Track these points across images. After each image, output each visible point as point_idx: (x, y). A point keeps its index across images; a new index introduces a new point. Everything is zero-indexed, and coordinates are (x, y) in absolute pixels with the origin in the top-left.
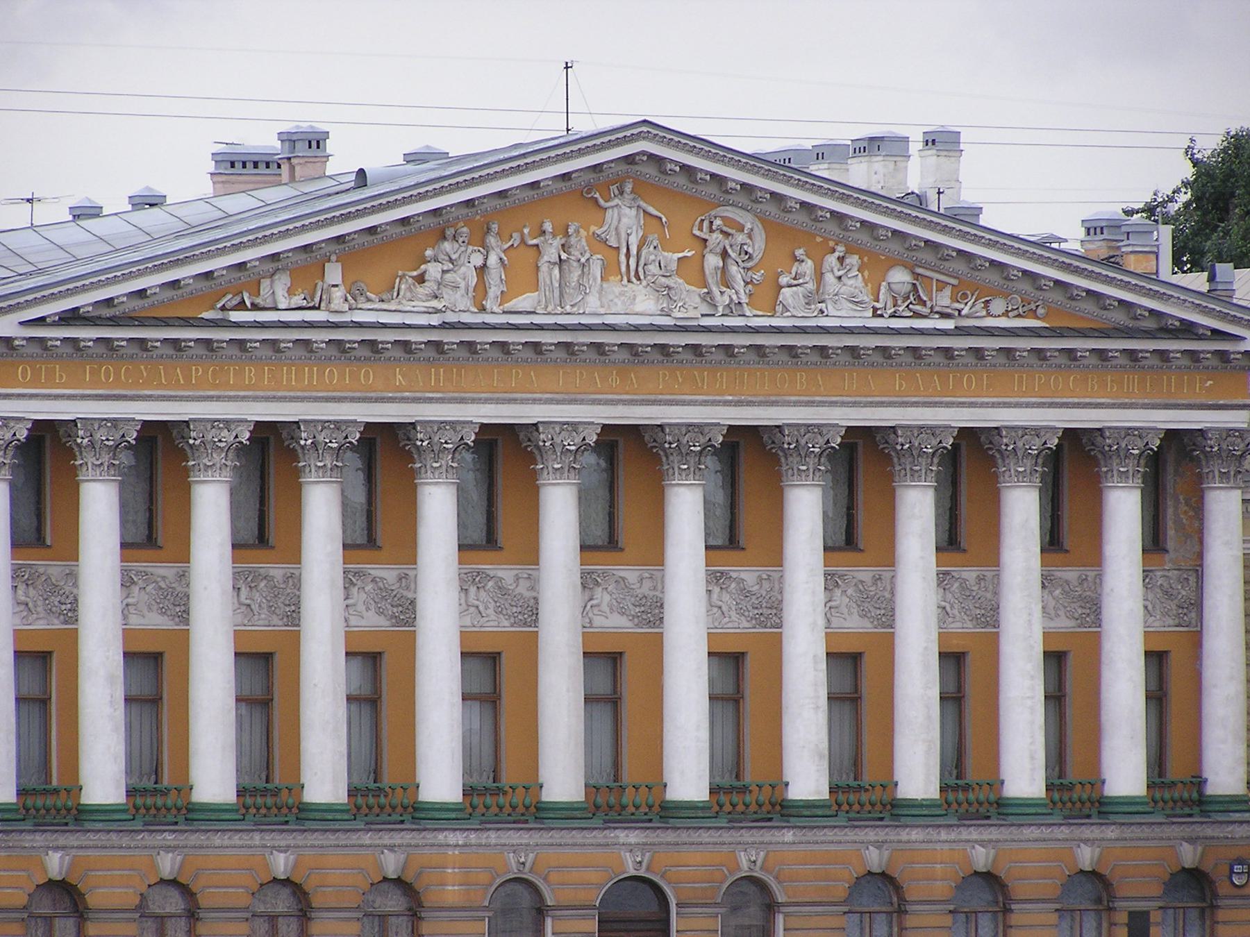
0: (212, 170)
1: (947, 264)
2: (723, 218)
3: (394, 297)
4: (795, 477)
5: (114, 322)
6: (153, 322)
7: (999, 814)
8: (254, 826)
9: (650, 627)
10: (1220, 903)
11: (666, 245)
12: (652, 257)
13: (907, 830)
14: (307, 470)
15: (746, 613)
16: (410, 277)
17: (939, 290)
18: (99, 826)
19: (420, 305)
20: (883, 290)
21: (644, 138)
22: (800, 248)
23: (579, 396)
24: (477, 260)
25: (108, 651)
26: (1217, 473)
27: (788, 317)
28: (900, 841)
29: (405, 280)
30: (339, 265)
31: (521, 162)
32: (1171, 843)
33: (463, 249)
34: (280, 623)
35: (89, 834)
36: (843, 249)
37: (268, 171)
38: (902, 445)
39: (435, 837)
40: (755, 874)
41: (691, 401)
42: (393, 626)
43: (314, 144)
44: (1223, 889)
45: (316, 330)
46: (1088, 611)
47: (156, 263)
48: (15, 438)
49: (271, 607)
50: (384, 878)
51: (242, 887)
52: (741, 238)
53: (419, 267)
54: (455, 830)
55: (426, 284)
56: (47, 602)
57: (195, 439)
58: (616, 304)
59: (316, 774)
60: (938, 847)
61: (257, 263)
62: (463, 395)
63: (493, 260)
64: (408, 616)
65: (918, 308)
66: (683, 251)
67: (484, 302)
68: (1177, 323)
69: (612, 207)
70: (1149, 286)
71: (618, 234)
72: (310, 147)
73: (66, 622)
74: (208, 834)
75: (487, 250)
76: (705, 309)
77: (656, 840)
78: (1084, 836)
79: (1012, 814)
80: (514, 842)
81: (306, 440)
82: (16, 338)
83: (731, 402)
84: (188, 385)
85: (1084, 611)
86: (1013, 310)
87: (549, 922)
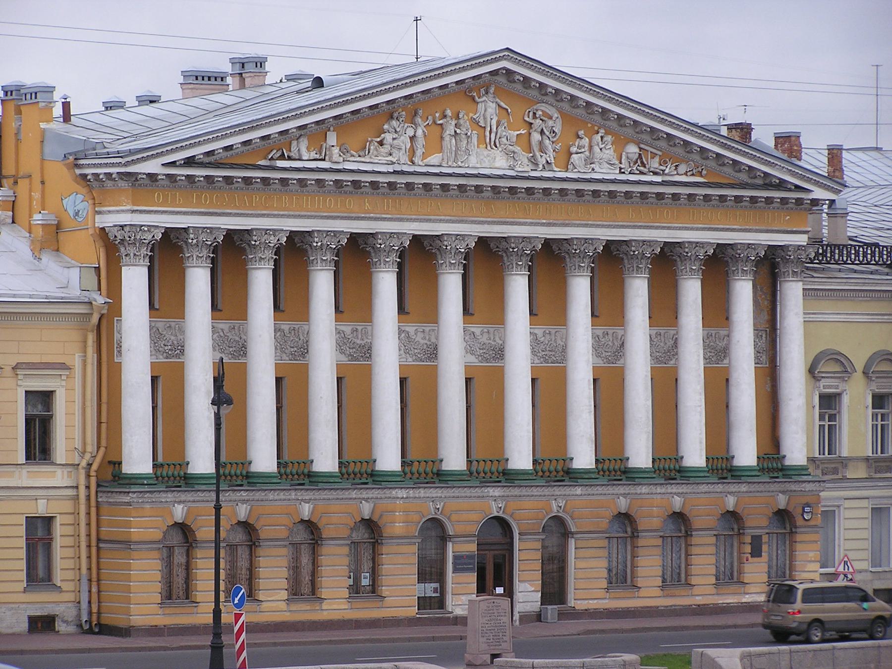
0: (182, 81)
1: (657, 142)
2: (542, 111)
3: (367, 154)
4: (577, 270)
5: (217, 165)
6: (251, 167)
7: (681, 477)
8: (546, 483)
9: (488, 362)
10: (798, 530)
11: (511, 127)
12: (504, 133)
13: (640, 486)
14: (315, 262)
15: (538, 354)
16: (376, 142)
17: (652, 158)
18: (203, 487)
19: (384, 159)
20: (624, 157)
21: (505, 59)
22: (581, 130)
23: (465, 218)
24: (410, 132)
25: (207, 375)
26: (791, 272)
27: (576, 172)
28: (636, 494)
29: (372, 144)
30: (335, 133)
31: (441, 72)
32: (773, 494)
33: (402, 125)
34: (287, 359)
35: (198, 493)
36: (604, 131)
37: (216, 83)
38: (634, 252)
39: (391, 493)
40: (560, 514)
41: (524, 222)
42: (349, 361)
43: (259, 65)
44: (799, 522)
45: (329, 173)
46: (713, 354)
47: (240, 128)
48: (154, 239)
49: (221, 349)
50: (362, 518)
51: (284, 525)
52: (550, 123)
53: (380, 136)
54: (402, 488)
55: (385, 146)
56: (157, 345)
57: (255, 241)
58: (485, 162)
59: (322, 454)
60: (655, 496)
61: (295, 130)
62: (402, 216)
63: (420, 132)
64: (358, 354)
65: (642, 168)
66: (520, 130)
67: (414, 159)
68: (777, 181)
69: (482, 102)
70: (766, 158)
71: (485, 118)
72: (256, 67)
73: (167, 358)
74: (266, 492)
75: (416, 125)
76: (531, 167)
77: (510, 494)
78: (730, 490)
79: (637, 478)
80: (434, 495)
81: (317, 243)
82: (159, 174)
83: (544, 223)
84: (251, 207)
85: (711, 354)
86: (690, 171)
87: (450, 546)
